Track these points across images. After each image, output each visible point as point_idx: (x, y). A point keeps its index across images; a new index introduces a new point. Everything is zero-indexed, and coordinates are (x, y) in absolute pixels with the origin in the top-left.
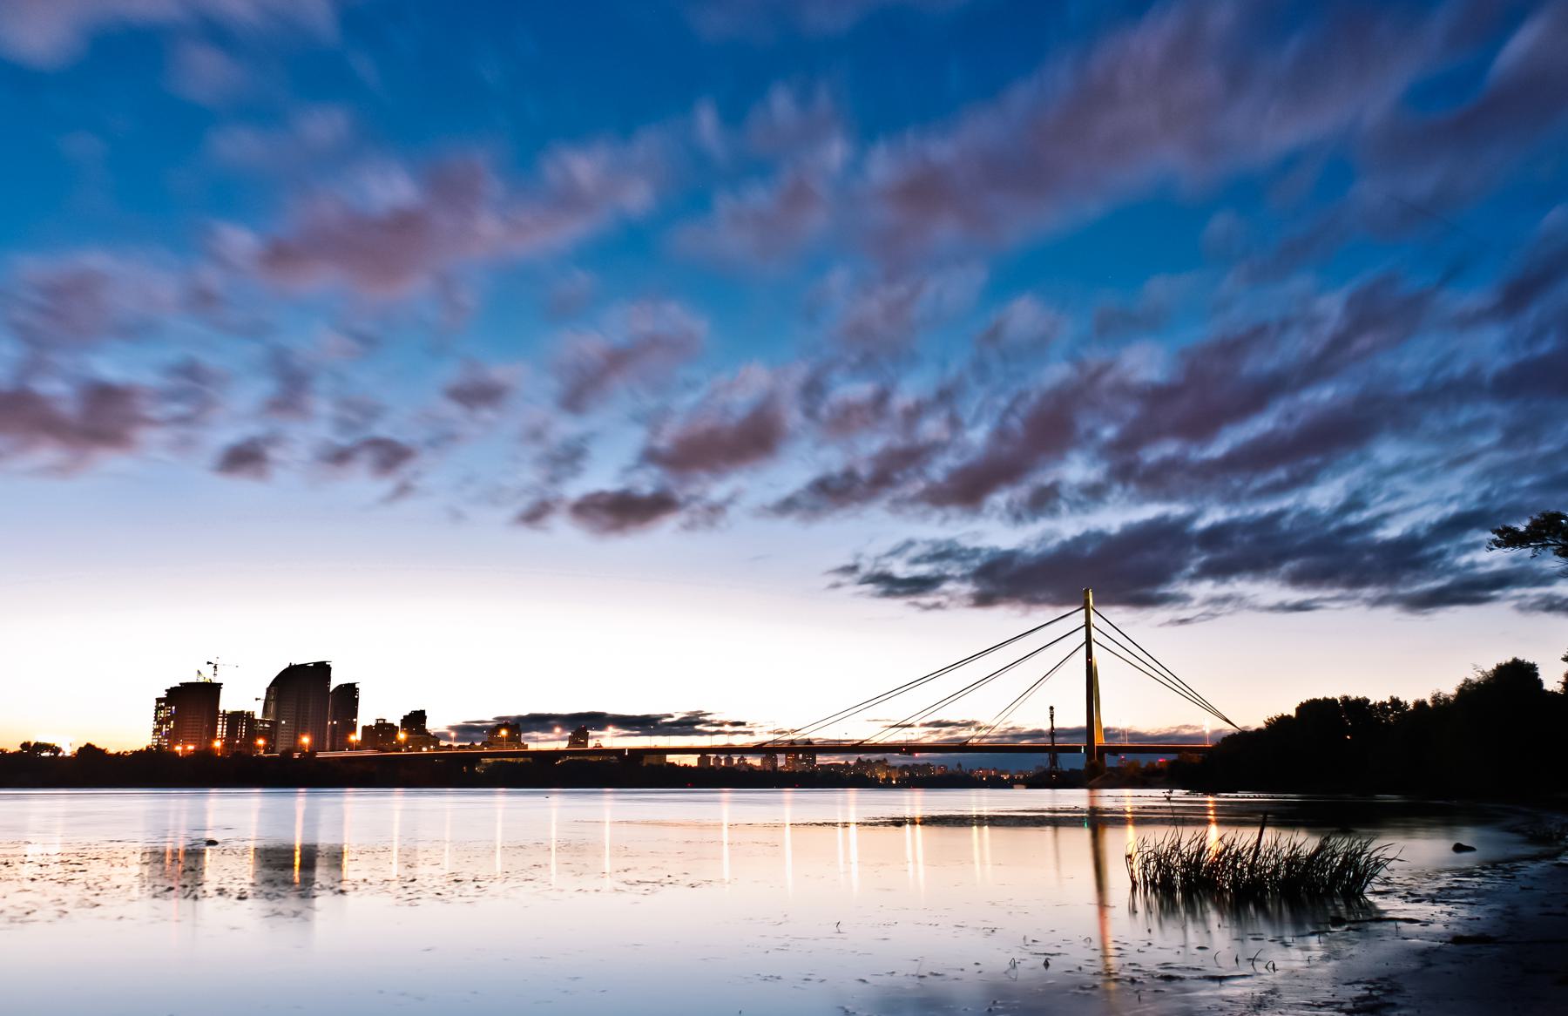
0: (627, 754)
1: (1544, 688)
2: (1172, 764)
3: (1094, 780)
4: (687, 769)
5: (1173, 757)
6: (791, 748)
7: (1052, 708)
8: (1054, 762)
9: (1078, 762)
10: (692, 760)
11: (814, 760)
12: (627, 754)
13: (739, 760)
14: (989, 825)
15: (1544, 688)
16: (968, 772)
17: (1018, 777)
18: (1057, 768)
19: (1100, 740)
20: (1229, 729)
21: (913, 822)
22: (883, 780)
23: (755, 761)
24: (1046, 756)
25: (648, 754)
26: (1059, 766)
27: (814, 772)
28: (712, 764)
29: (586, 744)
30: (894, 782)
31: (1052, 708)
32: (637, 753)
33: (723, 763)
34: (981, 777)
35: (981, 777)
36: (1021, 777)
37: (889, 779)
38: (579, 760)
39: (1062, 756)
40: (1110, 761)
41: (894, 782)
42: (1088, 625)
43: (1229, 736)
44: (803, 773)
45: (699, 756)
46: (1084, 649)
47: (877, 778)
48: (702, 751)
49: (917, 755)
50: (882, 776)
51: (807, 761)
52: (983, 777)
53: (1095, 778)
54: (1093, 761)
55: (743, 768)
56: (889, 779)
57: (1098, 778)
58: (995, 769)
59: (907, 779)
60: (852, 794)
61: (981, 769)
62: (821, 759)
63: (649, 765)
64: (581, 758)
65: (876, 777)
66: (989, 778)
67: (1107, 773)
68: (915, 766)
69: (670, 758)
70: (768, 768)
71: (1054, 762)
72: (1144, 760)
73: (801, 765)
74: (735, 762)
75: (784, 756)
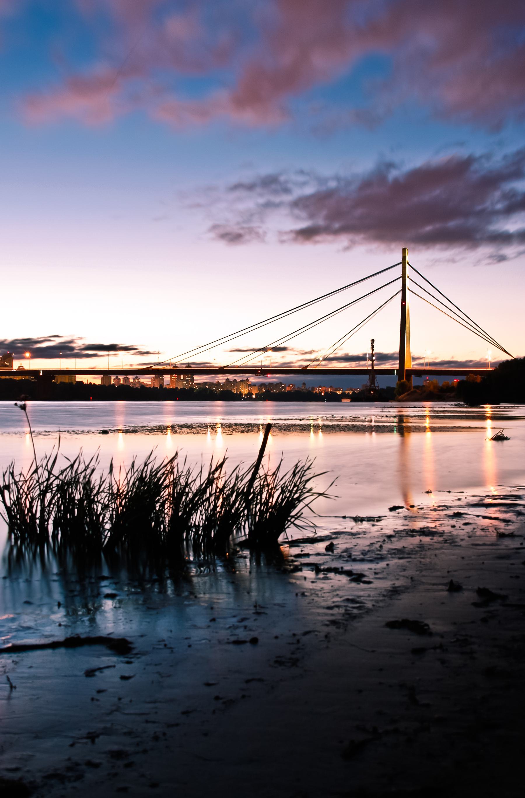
0: (41, 374)
1: (85, 383)
2: (461, 383)
3: (403, 396)
4: (91, 386)
5: (464, 378)
6: (175, 371)
7: (373, 341)
8: (373, 381)
9: (392, 382)
10: (97, 380)
11: (193, 380)
12: (41, 374)
13: (134, 379)
14: (377, 432)
15: (85, 383)
16: (310, 389)
17: (349, 393)
18: (375, 386)
19: (409, 365)
20: (505, 357)
21: (316, 427)
22: (246, 395)
23: (146, 380)
24: (367, 377)
25: (59, 375)
26: (376, 385)
27: (191, 389)
28: (112, 382)
29: (11, 366)
30: (254, 396)
31: (373, 341)
32: (50, 374)
33: (122, 382)
34: (321, 393)
35: (321, 393)
36: (351, 393)
37: (250, 394)
38: (5, 379)
39: (378, 376)
40: (415, 381)
41: (254, 396)
42: (404, 277)
43: (503, 362)
44: (183, 390)
45: (102, 376)
46: (400, 294)
47: (241, 394)
48: (106, 373)
49: (269, 375)
50: (245, 391)
51: (187, 381)
52: (322, 393)
53: (403, 393)
54: (402, 381)
55: (138, 386)
56: (250, 394)
57: (406, 393)
58: (331, 387)
59: (263, 394)
60: (219, 405)
61: (320, 387)
62: (199, 379)
63: (61, 383)
64: (7, 377)
65: (240, 392)
66: (326, 393)
67: (412, 390)
68: (270, 384)
69: (79, 378)
70: (157, 386)
71: (373, 381)
72: (441, 381)
73: (181, 383)
74: (131, 381)
75: (169, 376)
